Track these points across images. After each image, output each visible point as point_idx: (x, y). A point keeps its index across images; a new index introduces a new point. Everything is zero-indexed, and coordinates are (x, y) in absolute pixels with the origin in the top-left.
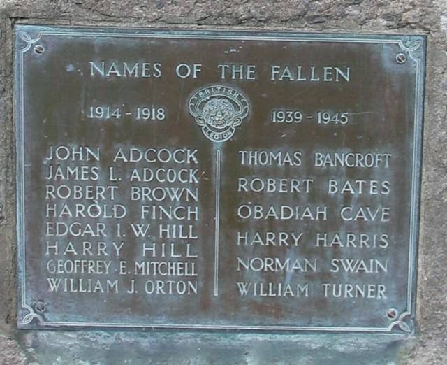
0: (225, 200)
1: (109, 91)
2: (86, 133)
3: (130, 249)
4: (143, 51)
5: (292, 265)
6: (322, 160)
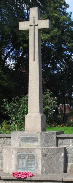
0: (27, 162)
1: (22, 156)
2: (21, 158)
3: (23, 164)
4: (23, 154)
5: (30, 165)
6: (31, 160)
